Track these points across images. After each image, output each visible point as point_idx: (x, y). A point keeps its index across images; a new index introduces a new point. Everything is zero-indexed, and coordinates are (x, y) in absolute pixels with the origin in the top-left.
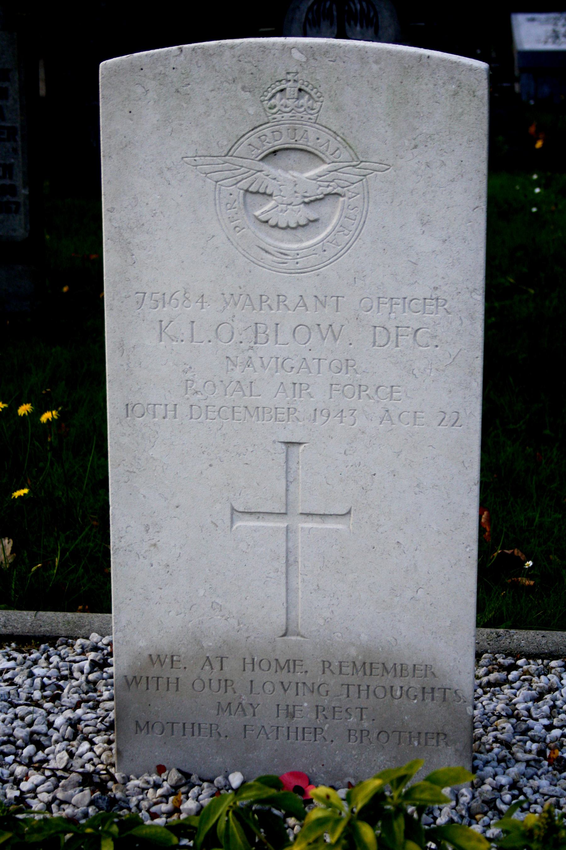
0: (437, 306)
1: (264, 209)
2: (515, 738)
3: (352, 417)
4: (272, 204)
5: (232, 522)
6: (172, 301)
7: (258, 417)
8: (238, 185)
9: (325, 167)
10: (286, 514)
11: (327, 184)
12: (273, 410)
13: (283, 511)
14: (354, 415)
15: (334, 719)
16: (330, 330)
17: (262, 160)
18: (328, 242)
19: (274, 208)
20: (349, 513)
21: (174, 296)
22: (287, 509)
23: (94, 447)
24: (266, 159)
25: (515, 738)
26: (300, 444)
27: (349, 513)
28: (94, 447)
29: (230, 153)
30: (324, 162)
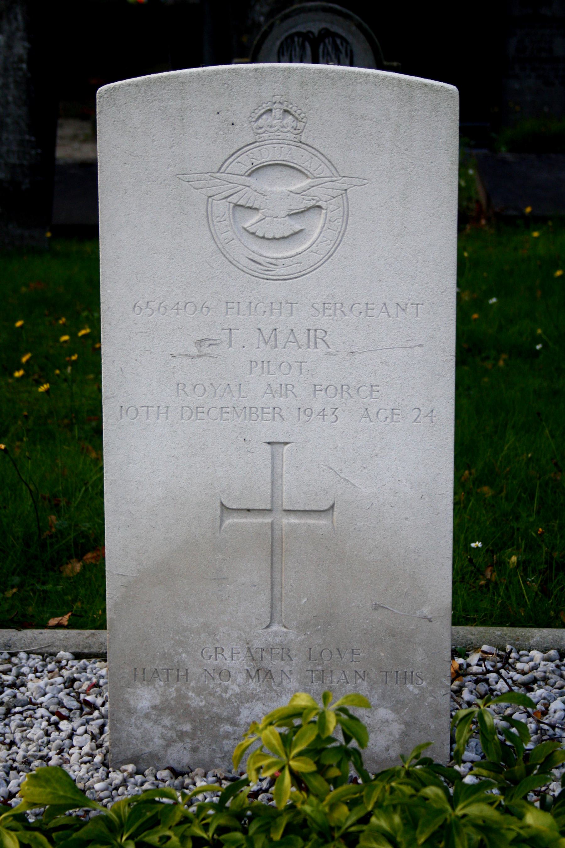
0: (335, 310)
1: (251, 221)
2: (421, 689)
3: (334, 416)
4: (257, 217)
5: (222, 521)
6: (204, 309)
7: (246, 417)
8: (229, 199)
9: (309, 181)
10: (270, 510)
11: (310, 198)
12: (260, 409)
13: (269, 507)
14: (335, 414)
15: (232, 660)
16: (274, 333)
17: (249, 175)
18: (312, 251)
19: (259, 221)
20: (332, 507)
21: (205, 305)
22: (272, 506)
23: (522, 585)
24: (255, 175)
25: (421, 689)
26: (287, 443)
27: (332, 507)
28: (522, 585)
29: (222, 170)
30: (308, 177)
